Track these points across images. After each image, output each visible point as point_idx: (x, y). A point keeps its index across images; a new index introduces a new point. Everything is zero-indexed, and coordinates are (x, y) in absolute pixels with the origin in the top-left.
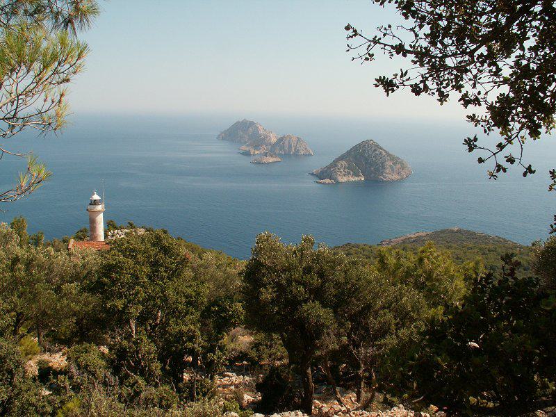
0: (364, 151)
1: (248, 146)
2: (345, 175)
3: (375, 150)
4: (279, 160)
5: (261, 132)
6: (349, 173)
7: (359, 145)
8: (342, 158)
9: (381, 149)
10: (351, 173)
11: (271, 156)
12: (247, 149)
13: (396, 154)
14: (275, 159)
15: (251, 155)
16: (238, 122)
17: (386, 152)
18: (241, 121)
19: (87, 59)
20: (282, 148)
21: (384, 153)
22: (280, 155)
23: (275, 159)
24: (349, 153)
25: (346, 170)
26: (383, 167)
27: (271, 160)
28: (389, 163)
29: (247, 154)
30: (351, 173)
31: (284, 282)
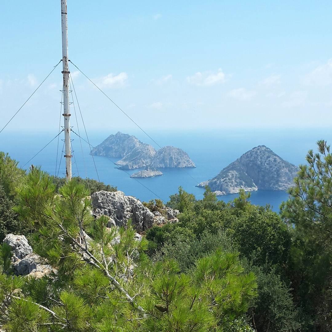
0: (256, 158)
1: (125, 160)
2: (236, 186)
3: (268, 157)
4: (161, 173)
5: (138, 145)
6: (241, 184)
7: (251, 151)
8: (232, 167)
9: (276, 155)
10: (244, 183)
11: (153, 169)
12: (124, 164)
13: (290, 161)
14: (157, 173)
15: (129, 169)
16: (112, 136)
17: (280, 158)
18: (114, 134)
19: (80, 177)
20: (163, 160)
21: (278, 160)
22: (161, 169)
23: (157, 173)
24: (240, 161)
25: (238, 181)
26: (279, 175)
27: (152, 174)
28: (285, 170)
29: (124, 168)
30: (244, 183)
31: (197, 225)
